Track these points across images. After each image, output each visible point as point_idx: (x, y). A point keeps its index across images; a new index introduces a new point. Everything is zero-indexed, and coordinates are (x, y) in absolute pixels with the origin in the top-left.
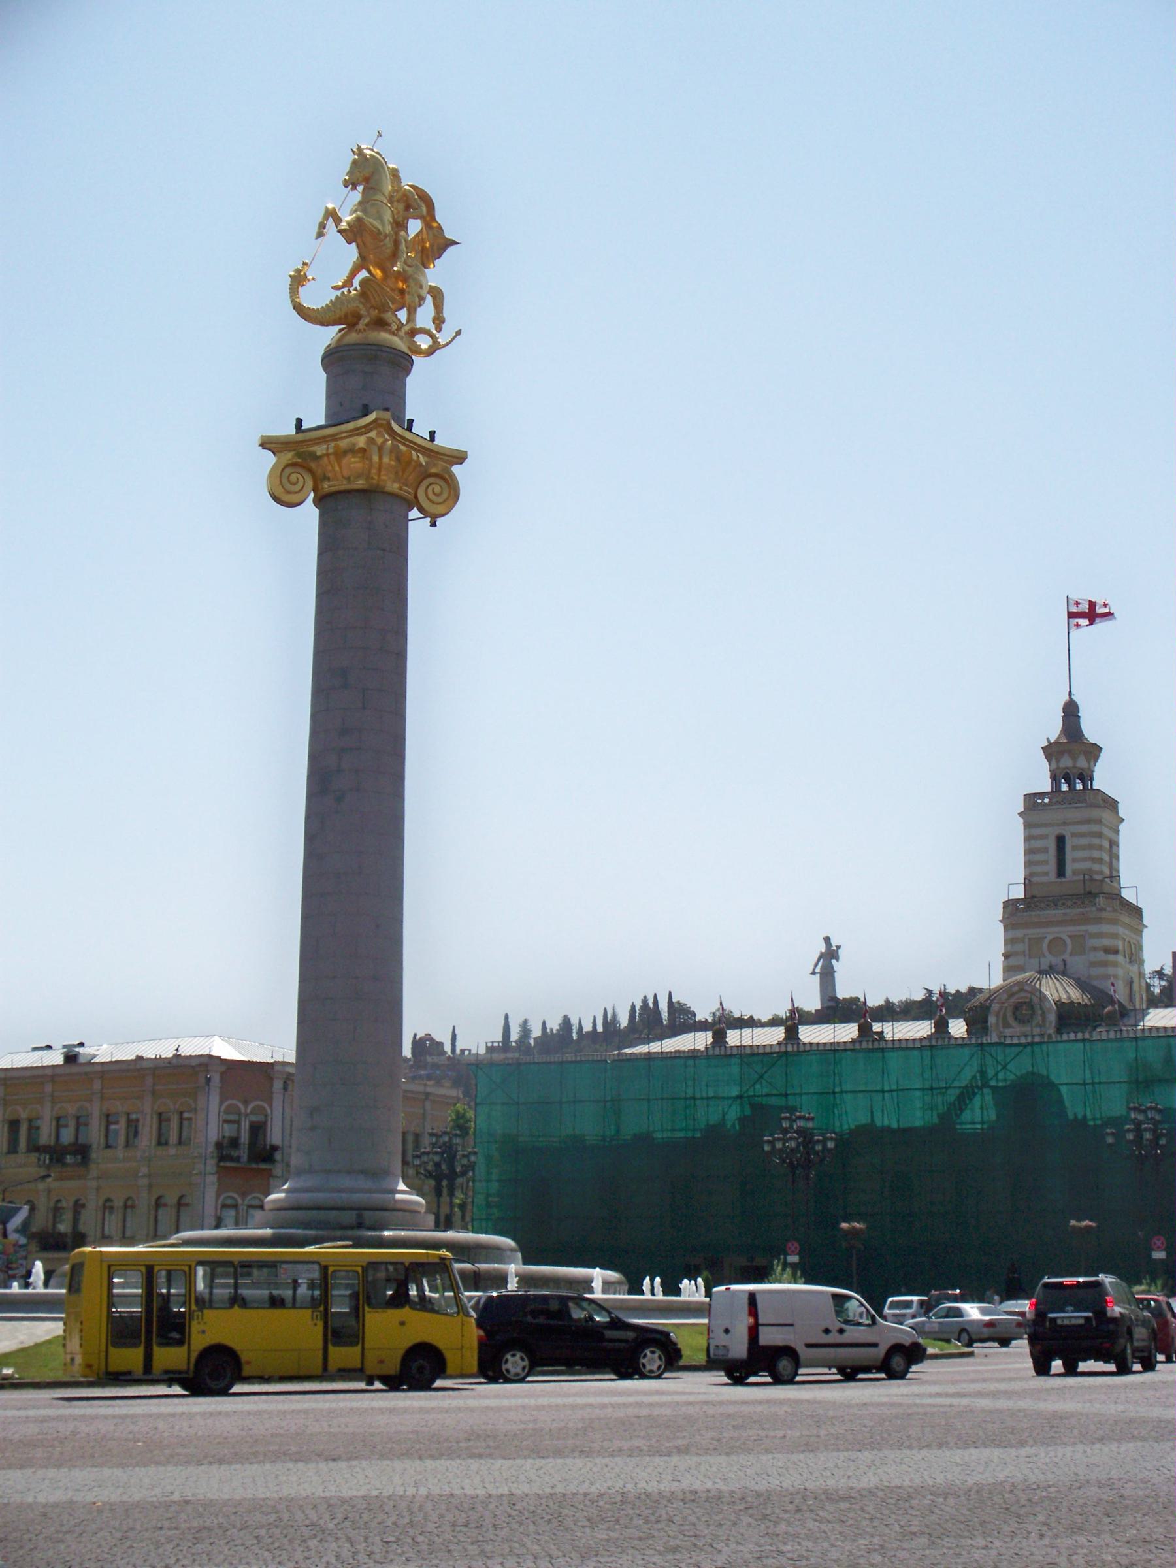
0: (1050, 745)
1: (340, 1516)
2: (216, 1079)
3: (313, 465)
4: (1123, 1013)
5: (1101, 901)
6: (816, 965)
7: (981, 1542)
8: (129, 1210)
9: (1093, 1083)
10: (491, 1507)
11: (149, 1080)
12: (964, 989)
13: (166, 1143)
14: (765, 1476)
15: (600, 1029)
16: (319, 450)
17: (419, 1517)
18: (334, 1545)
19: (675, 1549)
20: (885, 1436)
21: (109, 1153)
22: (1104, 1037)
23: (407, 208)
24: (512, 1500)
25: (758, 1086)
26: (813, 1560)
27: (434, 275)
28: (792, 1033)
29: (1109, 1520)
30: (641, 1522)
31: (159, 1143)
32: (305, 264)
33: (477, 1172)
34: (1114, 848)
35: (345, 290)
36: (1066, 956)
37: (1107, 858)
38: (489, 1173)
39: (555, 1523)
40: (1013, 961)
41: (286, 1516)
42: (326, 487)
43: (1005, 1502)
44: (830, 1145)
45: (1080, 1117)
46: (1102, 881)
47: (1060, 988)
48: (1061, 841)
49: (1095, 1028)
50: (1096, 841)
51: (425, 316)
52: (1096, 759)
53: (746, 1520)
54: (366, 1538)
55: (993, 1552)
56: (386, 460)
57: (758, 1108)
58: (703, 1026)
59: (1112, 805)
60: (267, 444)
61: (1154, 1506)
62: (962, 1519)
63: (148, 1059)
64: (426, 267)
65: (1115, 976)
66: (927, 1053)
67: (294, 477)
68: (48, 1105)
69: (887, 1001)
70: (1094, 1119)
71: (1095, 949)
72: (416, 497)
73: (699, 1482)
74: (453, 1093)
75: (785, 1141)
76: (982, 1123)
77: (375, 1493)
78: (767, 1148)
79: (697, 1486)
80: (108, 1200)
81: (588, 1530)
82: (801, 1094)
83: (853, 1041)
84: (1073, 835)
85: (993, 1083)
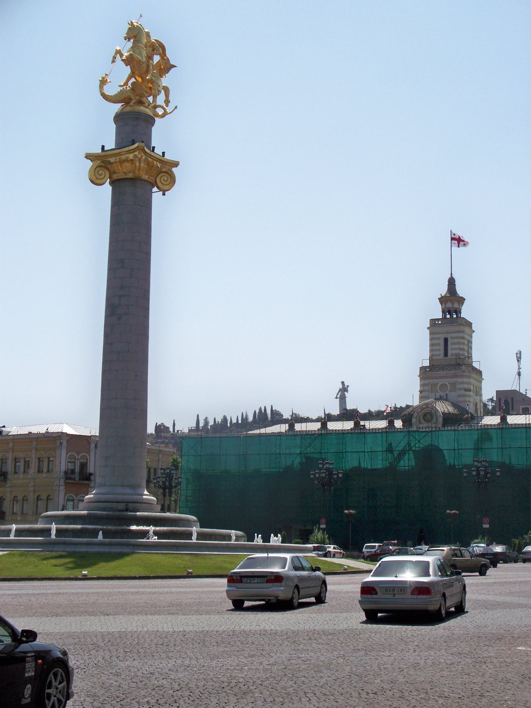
0: (442, 297)
1: (107, 640)
2: (65, 443)
3: (109, 167)
4: (473, 418)
5: (463, 367)
6: (338, 394)
7: (387, 653)
8: (25, 502)
9: (458, 449)
10: (175, 636)
11: (34, 443)
12: (404, 406)
13: (42, 472)
14: (297, 624)
15: (240, 422)
16: (112, 160)
17: (142, 640)
18: (102, 653)
19: (253, 656)
20: (354, 606)
21: (16, 476)
22: (464, 428)
23: (153, 50)
24: (184, 633)
25: (309, 449)
26: (312, 661)
27: (165, 81)
28: (324, 425)
29: (445, 644)
30: (239, 644)
31: (39, 472)
32: (106, 75)
33: (182, 486)
34: (470, 344)
35: (125, 87)
36: (447, 392)
37: (466, 348)
38: (187, 487)
39: (202, 644)
40: (424, 394)
41: (83, 640)
42: (115, 177)
43: (401, 636)
44: (340, 475)
45: (452, 464)
46: (464, 359)
47: (444, 407)
48: (446, 340)
49: (459, 425)
50: (462, 341)
51: (161, 99)
52: (463, 304)
53: (286, 643)
54: (117, 650)
55: (392, 658)
56: (142, 165)
57: (308, 458)
58: (285, 421)
59: (470, 324)
60: (88, 156)
61: (467, 638)
62: (381, 643)
63: (34, 434)
64: (161, 77)
65: (469, 401)
66: (384, 435)
67: (100, 172)
68: (34, 451)
69: (369, 411)
70: (459, 465)
71: (460, 389)
72: (156, 182)
73: (268, 626)
74: (172, 450)
75: (320, 473)
76: (408, 466)
77: (123, 630)
78: (312, 476)
79: (267, 628)
80: (16, 497)
81: (215, 647)
82: (328, 453)
83: (351, 429)
84: (452, 338)
85: (414, 448)
